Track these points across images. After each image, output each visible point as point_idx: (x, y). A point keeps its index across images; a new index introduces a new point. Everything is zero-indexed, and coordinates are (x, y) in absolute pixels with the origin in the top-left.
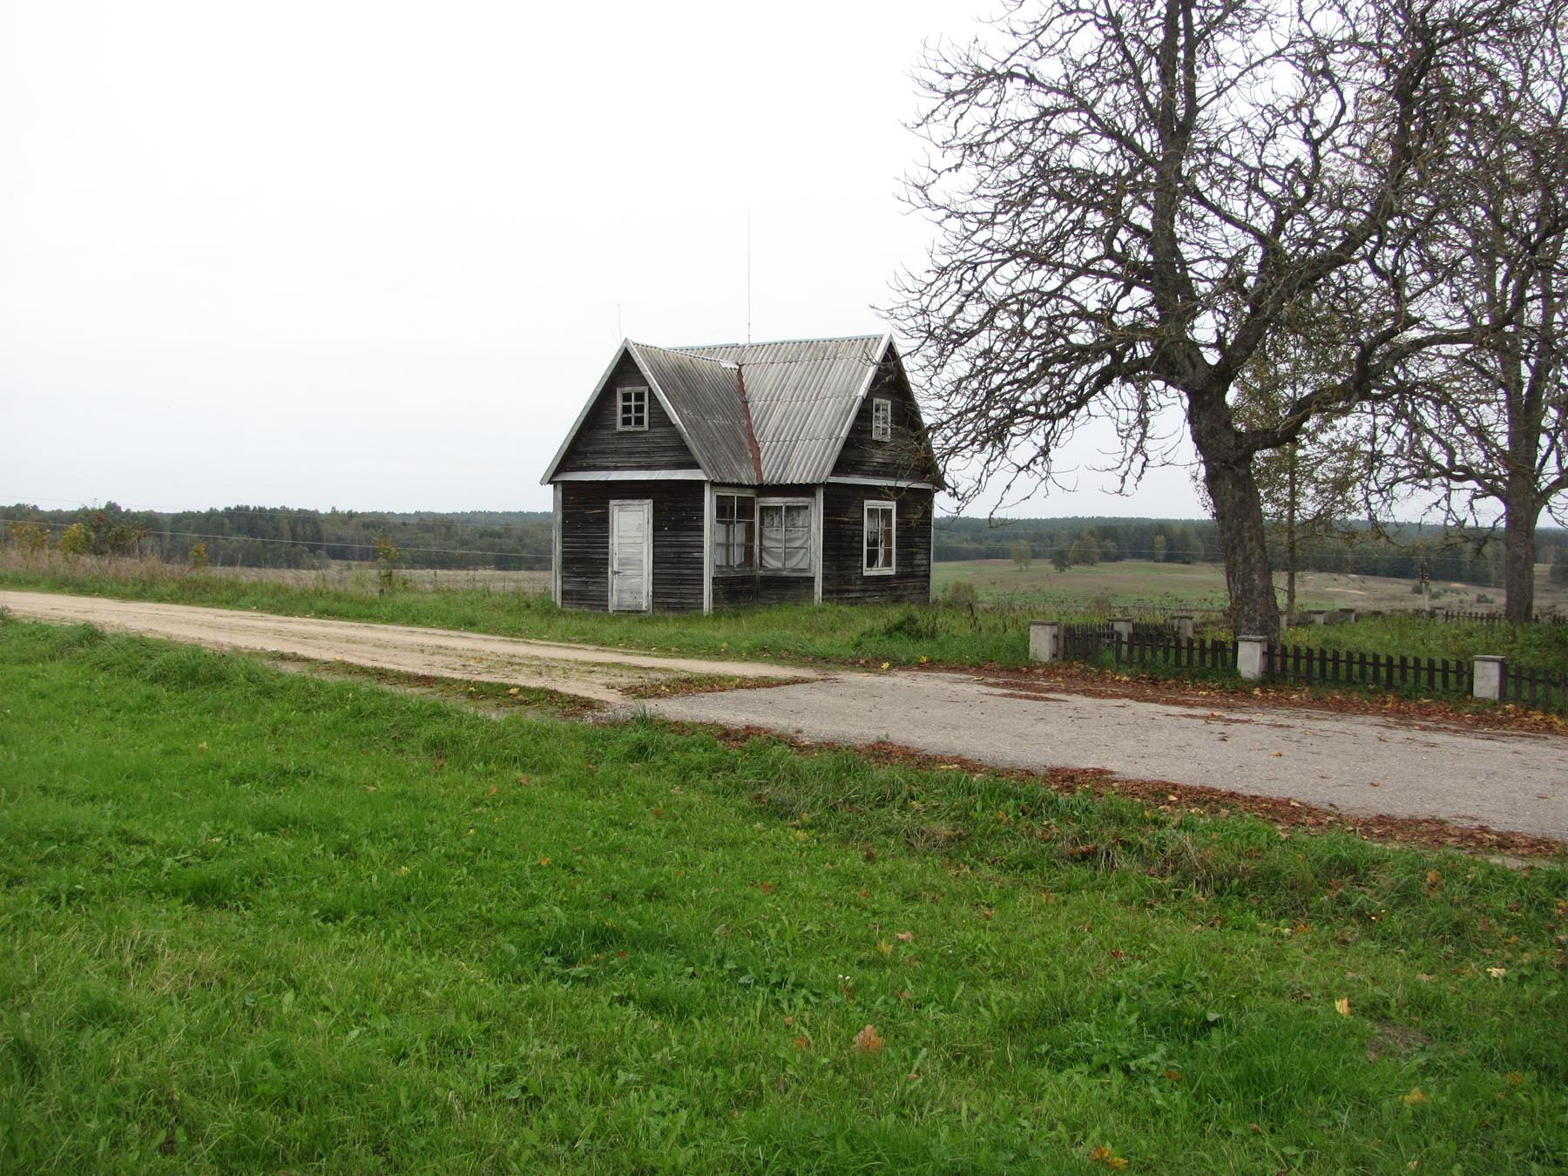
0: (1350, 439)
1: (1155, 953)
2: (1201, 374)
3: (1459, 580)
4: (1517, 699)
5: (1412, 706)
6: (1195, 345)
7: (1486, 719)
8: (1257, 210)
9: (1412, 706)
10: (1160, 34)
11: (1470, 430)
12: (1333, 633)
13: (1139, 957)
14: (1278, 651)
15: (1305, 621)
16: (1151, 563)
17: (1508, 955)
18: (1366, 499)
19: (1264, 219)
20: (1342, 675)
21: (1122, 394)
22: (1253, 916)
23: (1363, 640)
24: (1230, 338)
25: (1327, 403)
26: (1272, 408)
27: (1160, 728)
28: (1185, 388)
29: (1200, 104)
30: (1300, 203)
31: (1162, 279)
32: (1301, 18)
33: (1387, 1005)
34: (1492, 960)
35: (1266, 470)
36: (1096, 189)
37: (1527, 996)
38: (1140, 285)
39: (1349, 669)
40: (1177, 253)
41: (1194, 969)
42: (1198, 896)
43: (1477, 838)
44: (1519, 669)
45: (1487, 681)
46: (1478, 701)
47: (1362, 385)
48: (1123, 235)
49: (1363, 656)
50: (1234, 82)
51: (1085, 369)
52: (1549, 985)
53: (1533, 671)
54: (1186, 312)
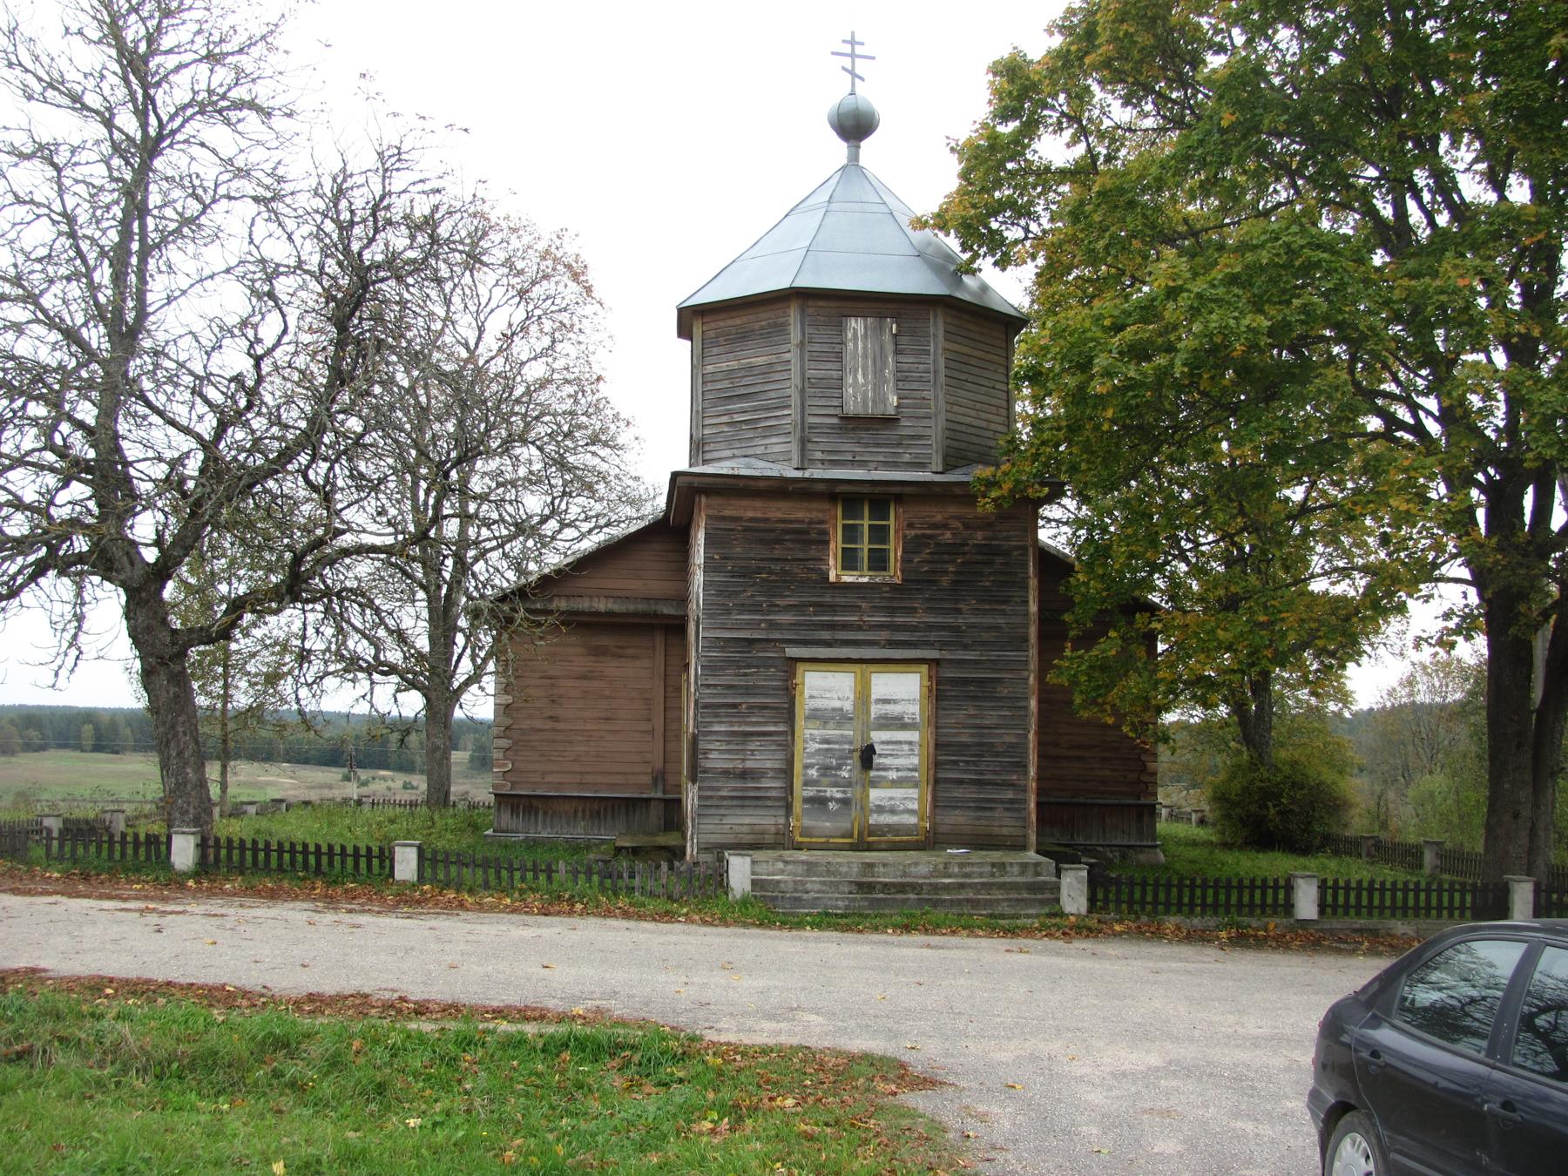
0: (283, 635)
1: (98, 1142)
2: (139, 571)
3: (387, 768)
4: (434, 880)
5: (339, 891)
6: (134, 544)
7: (408, 899)
8: (201, 418)
9: (339, 891)
10: (114, 236)
11: (391, 632)
12: (264, 824)
13: (82, 1147)
14: (211, 842)
15: (237, 812)
16: (78, 754)
17: (424, 1107)
18: (296, 692)
19: (207, 427)
20: (274, 863)
21: (56, 586)
22: (193, 1096)
23: (296, 829)
24: (168, 537)
25: (259, 602)
26: (208, 606)
27: (94, 923)
28: (123, 584)
29: (150, 310)
30: (240, 414)
31: (104, 477)
32: (251, 242)
33: (319, 1162)
34: (409, 1113)
35: (200, 662)
36: (38, 379)
37: (440, 1138)
38: (80, 480)
39: (280, 858)
40: (119, 450)
41: (136, 1151)
42: (138, 1084)
43: (397, 1008)
44: (435, 852)
45: (406, 864)
46: (399, 883)
47: (294, 589)
48: (65, 427)
49: (293, 845)
50: (184, 292)
51: (20, 560)
52: (457, 1128)
53: (447, 854)
54: (127, 511)
